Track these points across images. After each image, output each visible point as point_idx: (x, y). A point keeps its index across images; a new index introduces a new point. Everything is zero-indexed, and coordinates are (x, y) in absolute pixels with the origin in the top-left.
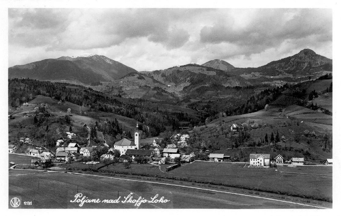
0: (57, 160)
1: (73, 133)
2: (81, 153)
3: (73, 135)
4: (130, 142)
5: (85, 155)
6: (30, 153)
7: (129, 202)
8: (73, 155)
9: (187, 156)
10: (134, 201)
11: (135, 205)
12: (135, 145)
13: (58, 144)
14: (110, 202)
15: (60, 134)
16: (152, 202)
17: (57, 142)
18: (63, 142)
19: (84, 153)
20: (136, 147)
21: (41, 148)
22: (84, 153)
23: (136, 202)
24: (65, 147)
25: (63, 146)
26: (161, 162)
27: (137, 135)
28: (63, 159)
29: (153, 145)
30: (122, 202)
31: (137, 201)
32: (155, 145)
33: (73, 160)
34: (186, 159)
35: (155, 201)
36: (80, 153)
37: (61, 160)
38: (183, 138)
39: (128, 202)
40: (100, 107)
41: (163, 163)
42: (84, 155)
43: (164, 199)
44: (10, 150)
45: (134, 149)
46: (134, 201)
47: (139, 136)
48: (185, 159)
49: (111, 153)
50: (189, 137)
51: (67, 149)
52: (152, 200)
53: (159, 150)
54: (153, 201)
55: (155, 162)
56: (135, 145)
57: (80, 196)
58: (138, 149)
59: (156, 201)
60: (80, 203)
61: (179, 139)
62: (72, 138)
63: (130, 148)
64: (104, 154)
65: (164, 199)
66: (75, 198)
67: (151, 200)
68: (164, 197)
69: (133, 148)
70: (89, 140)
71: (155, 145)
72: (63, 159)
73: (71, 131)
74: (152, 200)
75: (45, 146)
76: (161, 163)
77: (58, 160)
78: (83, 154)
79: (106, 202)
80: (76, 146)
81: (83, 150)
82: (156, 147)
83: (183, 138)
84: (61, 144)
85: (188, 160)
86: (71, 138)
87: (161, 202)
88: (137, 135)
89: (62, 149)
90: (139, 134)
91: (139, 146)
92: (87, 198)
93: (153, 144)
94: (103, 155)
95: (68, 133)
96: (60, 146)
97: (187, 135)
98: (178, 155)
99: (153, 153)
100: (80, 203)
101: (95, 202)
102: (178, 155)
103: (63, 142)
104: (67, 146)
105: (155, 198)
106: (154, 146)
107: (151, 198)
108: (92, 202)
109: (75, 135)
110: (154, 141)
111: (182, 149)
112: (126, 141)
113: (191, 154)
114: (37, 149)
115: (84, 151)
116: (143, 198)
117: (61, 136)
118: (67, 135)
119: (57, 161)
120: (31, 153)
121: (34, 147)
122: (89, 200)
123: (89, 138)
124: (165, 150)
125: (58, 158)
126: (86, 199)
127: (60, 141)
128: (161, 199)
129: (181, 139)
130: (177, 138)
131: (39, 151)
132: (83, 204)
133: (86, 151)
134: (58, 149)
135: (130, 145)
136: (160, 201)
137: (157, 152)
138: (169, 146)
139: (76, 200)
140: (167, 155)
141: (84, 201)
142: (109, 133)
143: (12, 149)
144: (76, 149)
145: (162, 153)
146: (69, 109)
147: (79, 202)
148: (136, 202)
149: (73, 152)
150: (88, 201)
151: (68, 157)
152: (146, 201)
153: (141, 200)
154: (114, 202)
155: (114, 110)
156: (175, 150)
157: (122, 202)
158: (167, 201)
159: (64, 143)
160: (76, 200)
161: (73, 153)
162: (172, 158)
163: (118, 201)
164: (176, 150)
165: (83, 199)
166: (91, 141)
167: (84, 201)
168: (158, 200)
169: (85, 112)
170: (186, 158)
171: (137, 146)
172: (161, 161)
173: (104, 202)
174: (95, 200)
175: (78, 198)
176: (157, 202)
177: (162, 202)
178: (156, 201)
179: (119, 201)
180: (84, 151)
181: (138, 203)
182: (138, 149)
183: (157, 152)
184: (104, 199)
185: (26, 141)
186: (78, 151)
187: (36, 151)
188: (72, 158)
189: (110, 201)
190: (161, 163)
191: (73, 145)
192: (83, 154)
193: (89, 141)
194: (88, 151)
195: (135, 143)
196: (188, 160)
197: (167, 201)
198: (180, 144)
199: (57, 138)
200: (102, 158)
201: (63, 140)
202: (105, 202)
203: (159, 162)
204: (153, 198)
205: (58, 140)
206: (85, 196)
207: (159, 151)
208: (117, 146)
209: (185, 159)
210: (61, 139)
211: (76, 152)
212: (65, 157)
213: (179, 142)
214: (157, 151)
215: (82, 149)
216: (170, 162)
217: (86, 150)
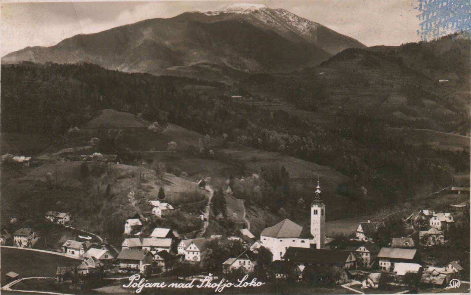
0: (121, 269)
1: (165, 204)
2: (181, 251)
3: (165, 208)
4: (298, 228)
5: (189, 257)
6: (66, 248)
7: (207, 287)
8: (160, 258)
9: (439, 270)
10: (214, 285)
11: (216, 291)
12: (312, 237)
13: (128, 230)
14: (180, 287)
15: (136, 205)
16: (239, 286)
17: (126, 225)
18: (140, 224)
19: (186, 253)
20: (313, 242)
21: (90, 238)
22: (186, 253)
23: (217, 286)
24: (142, 237)
25: (138, 234)
26: (367, 283)
27: (316, 212)
28: (133, 266)
29: (358, 238)
30: (198, 286)
31: (219, 286)
32: (361, 237)
33: (159, 269)
34: (435, 278)
35: (244, 284)
36: (179, 253)
37: (129, 269)
38: (437, 221)
39: (205, 287)
40: (250, 137)
41: (373, 285)
42: (186, 258)
43: (257, 282)
44: (22, 241)
45: (308, 246)
46: (214, 285)
47: (322, 214)
48: (432, 278)
49: (250, 255)
50: (452, 220)
51: (148, 242)
52: (240, 283)
53: (367, 251)
54: (241, 285)
55: (355, 282)
56: (312, 237)
57: (137, 278)
58: (318, 247)
59: (246, 285)
60: (137, 288)
61: (425, 224)
62: (162, 216)
63: (298, 243)
64: (233, 256)
65: (257, 282)
66: (130, 281)
67: (238, 283)
68: (256, 278)
69: (307, 244)
70: (205, 219)
71: (361, 237)
72: (133, 266)
73: (161, 197)
74: (240, 283)
75: (99, 234)
76: (368, 285)
77: (123, 269)
78: (184, 256)
79: (174, 286)
80: (169, 235)
81: (185, 246)
82: (362, 243)
83: (437, 221)
84: (136, 228)
85: (439, 281)
86: (160, 217)
87: (252, 286)
88: (316, 212)
89: (136, 242)
90: (322, 211)
91: (322, 240)
92: (147, 281)
93: (358, 235)
94: (229, 261)
95: (155, 203)
96: (132, 235)
97: (447, 215)
98: (415, 268)
99: (351, 258)
100: (137, 288)
101: (158, 287)
102: (415, 268)
103: (140, 224)
104: (147, 234)
105: (243, 280)
106: (360, 240)
107: (238, 280)
108: (154, 286)
109: (171, 207)
110: (360, 228)
111: (429, 249)
112: (289, 225)
113: (450, 266)
114: (80, 240)
115: (188, 249)
116: (227, 281)
117: (138, 209)
118: (153, 207)
119: (120, 271)
120: (68, 250)
121: (75, 235)
122: (149, 284)
123: (205, 216)
124: (384, 252)
125: (122, 265)
126: (145, 282)
127: (132, 222)
128: (253, 281)
129: (431, 224)
130: (420, 221)
131: (84, 246)
132: (141, 289)
133: (193, 249)
134: (127, 243)
135: (301, 237)
136: (251, 284)
137: (364, 256)
138: (394, 241)
139: (132, 284)
140: (387, 265)
141: (143, 286)
142: (261, 205)
143: (25, 239)
144: (168, 242)
145: (376, 260)
146: (172, 143)
147: (135, 287)
148: (217, 286)
149: (160, 250)
150: (148, 285)
151: (145, 261)
152: (231, 284)
153: (223, 284)
154: (186, 287)
155: (283, 146)
156: (410, 254)
157: (198, 286)
158: (261, 283)
159: (141, 226)
160: (132, 284)
161: (160, 254)
162: (398, 274)
163: (192, 285)
164: (410, 254)
165: (141, 282)
166: (210, 222)
167: (143, 286)
168: (247, 284)
169: (211, 151)
170: (434, 276)
171: (317, 241)
172: (369, 280)
173: (171, 286)
174: (159, 284)
175: (135, 281)
176: (247, 286)
177: (254, 285)
178: (246, 285)
179: (193, 286)
180: (188, 249)
181: (220, 287)
182: (318, 247)
183: (364, 256)
184: (171, 283)
185: (60, 220)
186: (174, 247)
187: (78, 244)
188: (155, 263)
189: (181, 285)
190: (368, 285)
191: (161, 232)
192: (184, 256)
193: (206, 224)
194: (198, 250)
195: (313, 232)
196: (439, 281)
197: (261, 283)
198: (426, 237)
199: (127, 216)
200: (227, 266)
201: (141, 220)
202: (172, 287)
203: (364, 283)
204: (241, 280)
205: (130, 221)
206: (144, 279)
207: (369, 254)
208: (267, 238)
209: (432, 278)
210: (137, 216)
211: (168, 250)
212: (137, 262)
213: (422, 233)
214: (365, 254)
215: (182, 244)
216: (393, 284)
217: (193, 246)
